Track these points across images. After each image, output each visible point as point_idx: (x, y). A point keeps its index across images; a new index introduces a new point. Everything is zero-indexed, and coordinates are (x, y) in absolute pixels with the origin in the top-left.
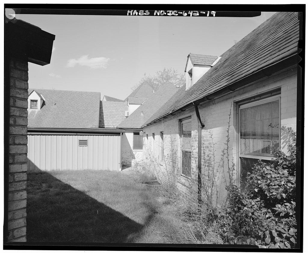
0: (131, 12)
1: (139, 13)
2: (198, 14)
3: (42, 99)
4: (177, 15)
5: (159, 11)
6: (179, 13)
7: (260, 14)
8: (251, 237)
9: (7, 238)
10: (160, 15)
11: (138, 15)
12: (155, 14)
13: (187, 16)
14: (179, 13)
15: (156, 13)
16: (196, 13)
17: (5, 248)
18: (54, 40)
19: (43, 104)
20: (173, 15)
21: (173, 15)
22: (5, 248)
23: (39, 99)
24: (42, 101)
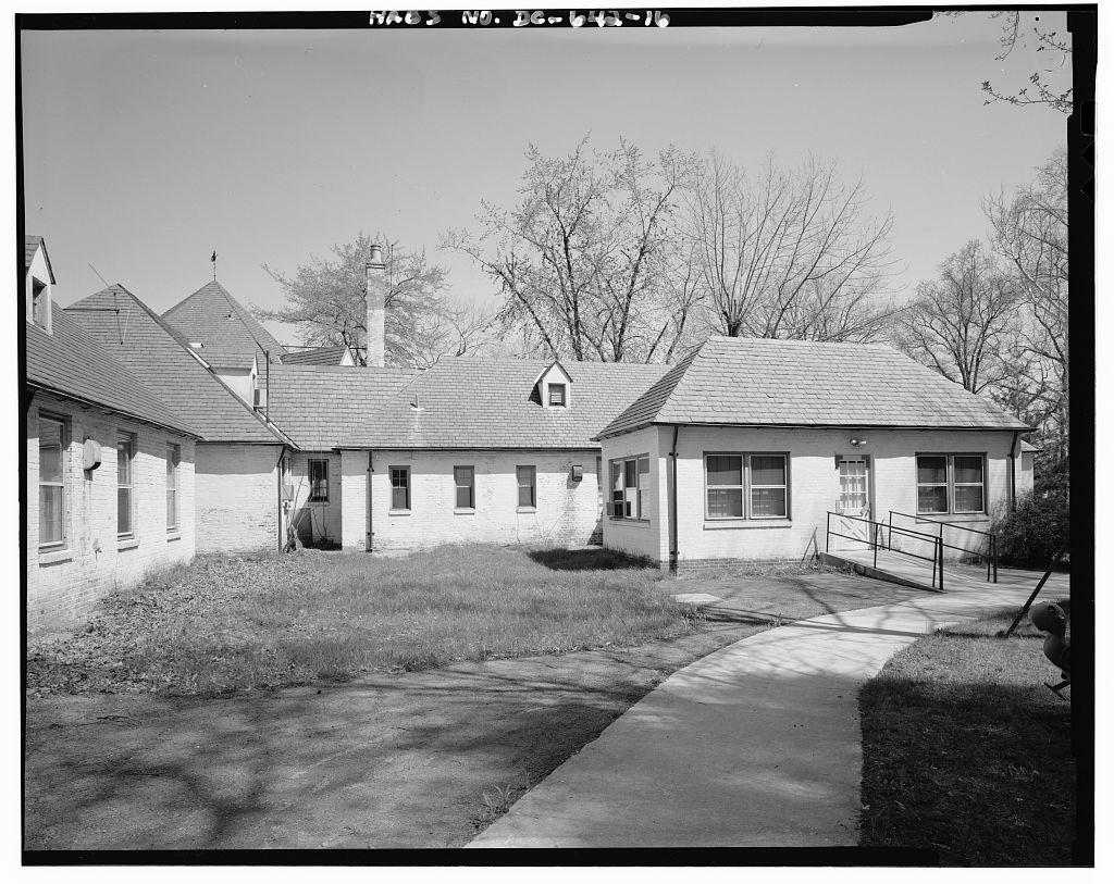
7: (929, 17)
12: (371, 22)
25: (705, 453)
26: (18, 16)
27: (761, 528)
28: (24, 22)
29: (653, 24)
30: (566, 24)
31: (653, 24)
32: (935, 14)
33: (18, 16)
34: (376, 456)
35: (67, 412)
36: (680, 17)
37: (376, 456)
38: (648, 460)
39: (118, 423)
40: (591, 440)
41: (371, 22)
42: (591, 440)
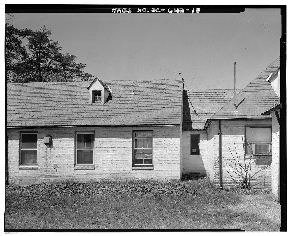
0: (115, 10)
1: (121, 10)
2: (184, 12)
3: (106, 89)
4: (160, 11)
5: (141, 9)
6: (161, 10)
7: (244, 10)
8: (47, 47)
9: (25, 32)
10: (142, 12)
11: (122, 12)
12: (138, 12)
13: (184, 13)
14: (161, 10)
15: (139, 11)
16: (182, 10)
17: (6, 230)
18: (281, 38)
19: (109, 98)
20: (156, 12)
21: (156, 12)
22: (6, 230)
23: (103, 89)
24: (108, 94)
25: (190, 134)
26: (285, 6)
27: (148, 170)
28: (283, 8)
29: (195, 12)
30: (166, 11)
31: (195, 12)
32: (246, 9)
33: (285, 6)
34: (222, 121)
35: (37, 131)
36: (206, 9)
37: (222, 122)
38: (91, 152)
39: (72, 131)
40: (262, 114)
41: (138, 12)
42: (262, 114)
